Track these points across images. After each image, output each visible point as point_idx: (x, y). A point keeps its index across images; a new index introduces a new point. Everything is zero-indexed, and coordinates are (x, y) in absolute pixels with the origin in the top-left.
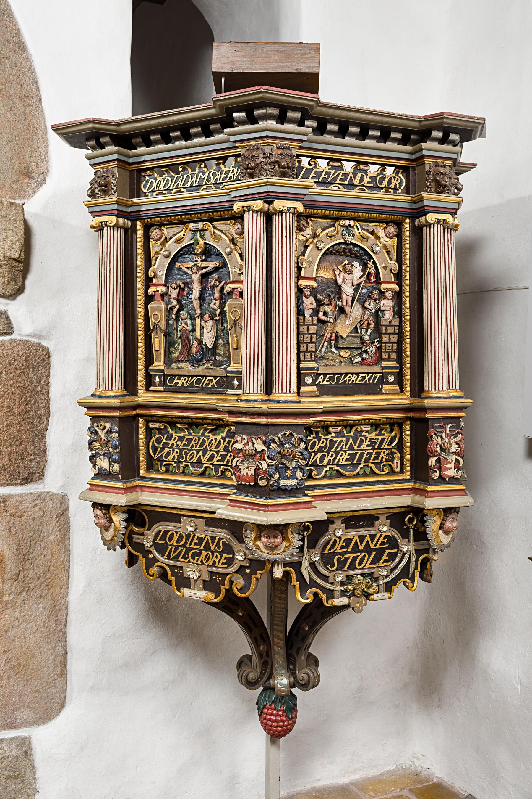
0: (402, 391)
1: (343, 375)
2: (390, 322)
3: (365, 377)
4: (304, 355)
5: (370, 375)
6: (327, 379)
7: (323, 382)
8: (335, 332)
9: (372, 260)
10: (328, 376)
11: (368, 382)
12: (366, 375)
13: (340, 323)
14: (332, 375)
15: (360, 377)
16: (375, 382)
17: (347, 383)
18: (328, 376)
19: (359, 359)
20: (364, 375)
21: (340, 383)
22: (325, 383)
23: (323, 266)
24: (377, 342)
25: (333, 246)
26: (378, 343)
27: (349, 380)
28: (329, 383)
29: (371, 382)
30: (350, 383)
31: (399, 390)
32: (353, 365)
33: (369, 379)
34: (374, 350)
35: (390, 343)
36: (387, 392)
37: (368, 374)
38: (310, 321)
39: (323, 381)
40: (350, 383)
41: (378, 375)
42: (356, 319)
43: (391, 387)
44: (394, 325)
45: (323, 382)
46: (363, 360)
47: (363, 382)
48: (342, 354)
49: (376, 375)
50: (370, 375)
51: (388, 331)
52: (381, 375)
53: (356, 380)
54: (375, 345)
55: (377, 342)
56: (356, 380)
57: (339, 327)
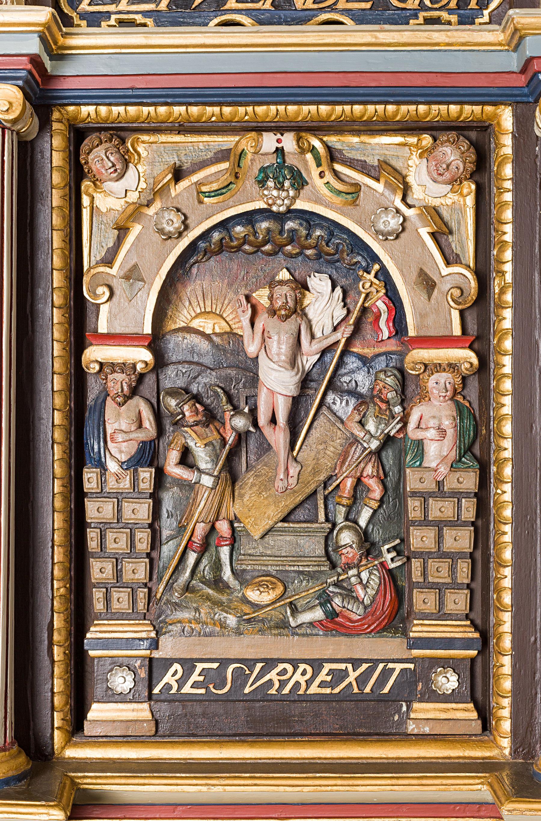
0: (486, 726)
1: (259, 666)
2: (440, 484)
3: (345, 674)
4: (108, 600)
5: (365, 666)
6: (195, 677)
7: (180, 688)
8: (232, 517)
9: (377, 267)
10: (327, 667)
11: (356, 690)
12: (350, 666)
13: (253, 485)
14: (215, 665)
15: (325, 671)
16: (386, 690)
17: (273, 691)
18: (200, 666)
19: (318, 614)
20: (342, 666)
21: (247, 690)
22: (187, 689)
23: (199, 293)
24: (389, 551)
25: (223, 225)
26: (394, 554)
27: (283, 684)
28: (203, 691)
29: (368, 690)
30: (286, 691)
31: (477, 726)
32: (294, 634)
33: (362, 680)
34: (375, 582)
35: (442, 555)
36: (427, 730)
37: (356, 663)
38: (126, 483)
39: (181, 683)
40: (286, 691)
41: (399, 667)
42: (315, 472)
43: (446, 710)
44: (458, 495)
45: (180, 688)
46: (332, 615)
47: (337, 690)
48: (253, 595)
49: (391, 665)
50: (365, 666)
51: (434, 514)
52: (412, 666)
53: (309, 683)
54: (382, 564)
55: (389, 551)
56: (309, 683)
57: (246, 498)
